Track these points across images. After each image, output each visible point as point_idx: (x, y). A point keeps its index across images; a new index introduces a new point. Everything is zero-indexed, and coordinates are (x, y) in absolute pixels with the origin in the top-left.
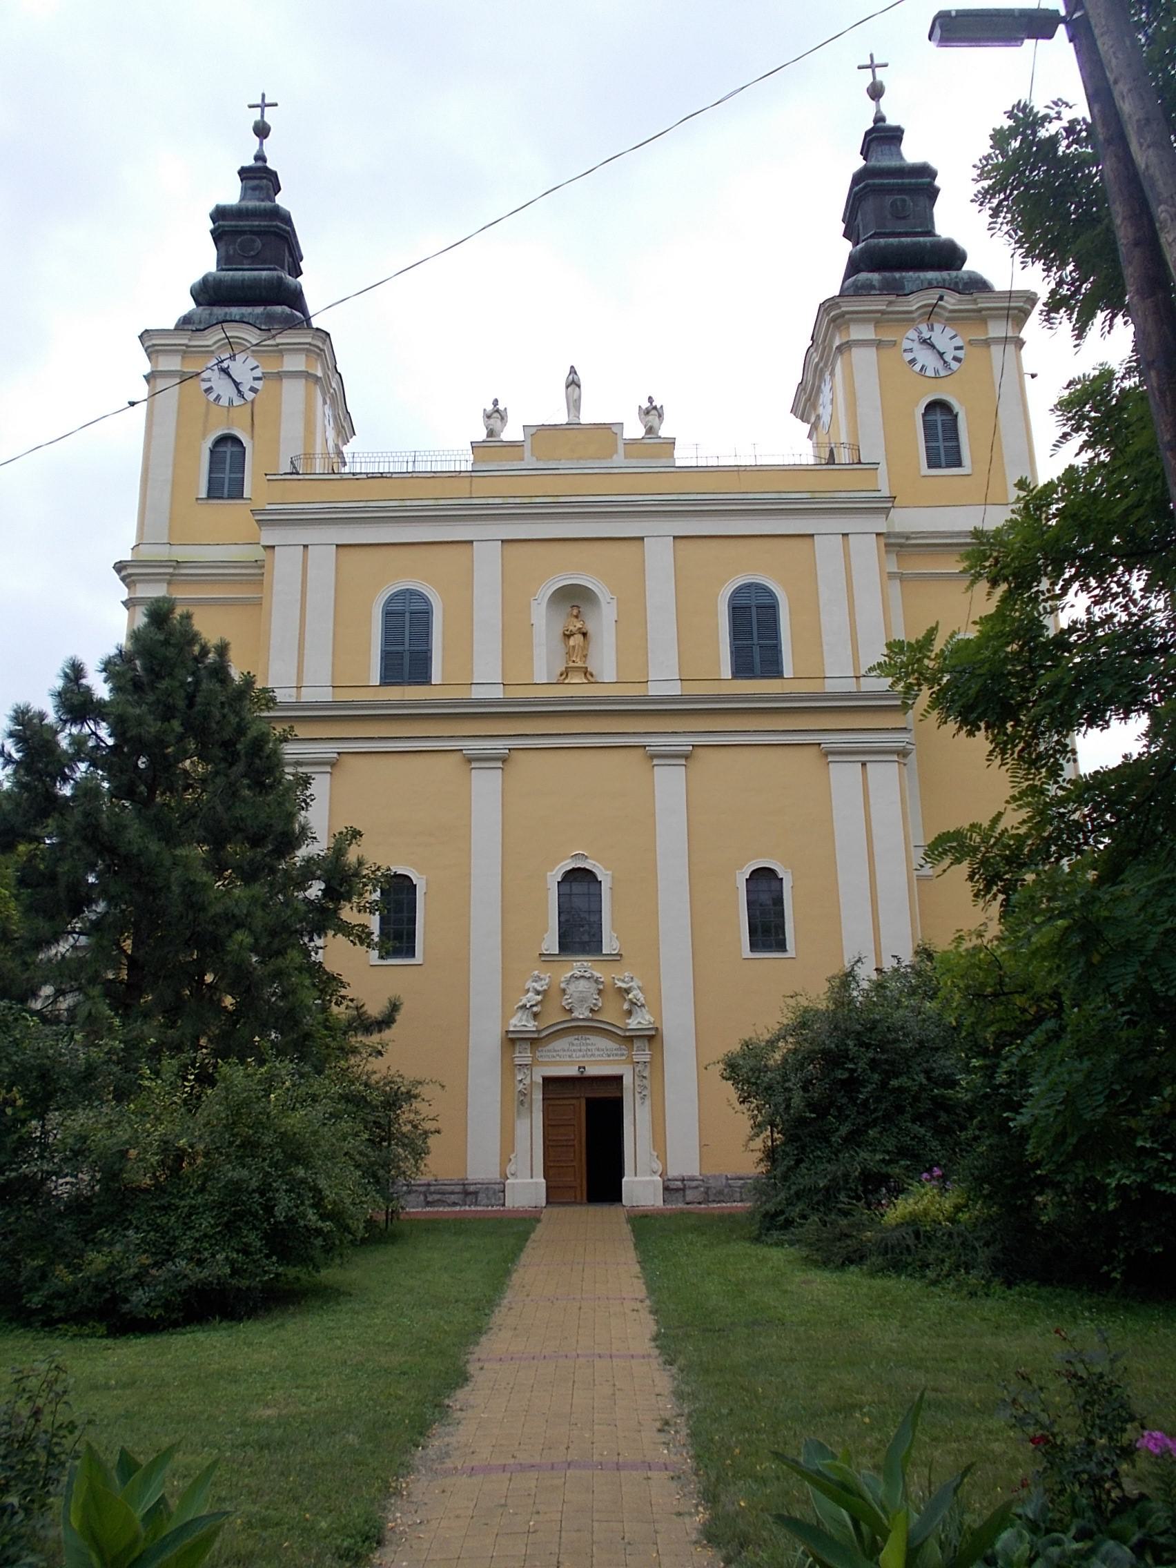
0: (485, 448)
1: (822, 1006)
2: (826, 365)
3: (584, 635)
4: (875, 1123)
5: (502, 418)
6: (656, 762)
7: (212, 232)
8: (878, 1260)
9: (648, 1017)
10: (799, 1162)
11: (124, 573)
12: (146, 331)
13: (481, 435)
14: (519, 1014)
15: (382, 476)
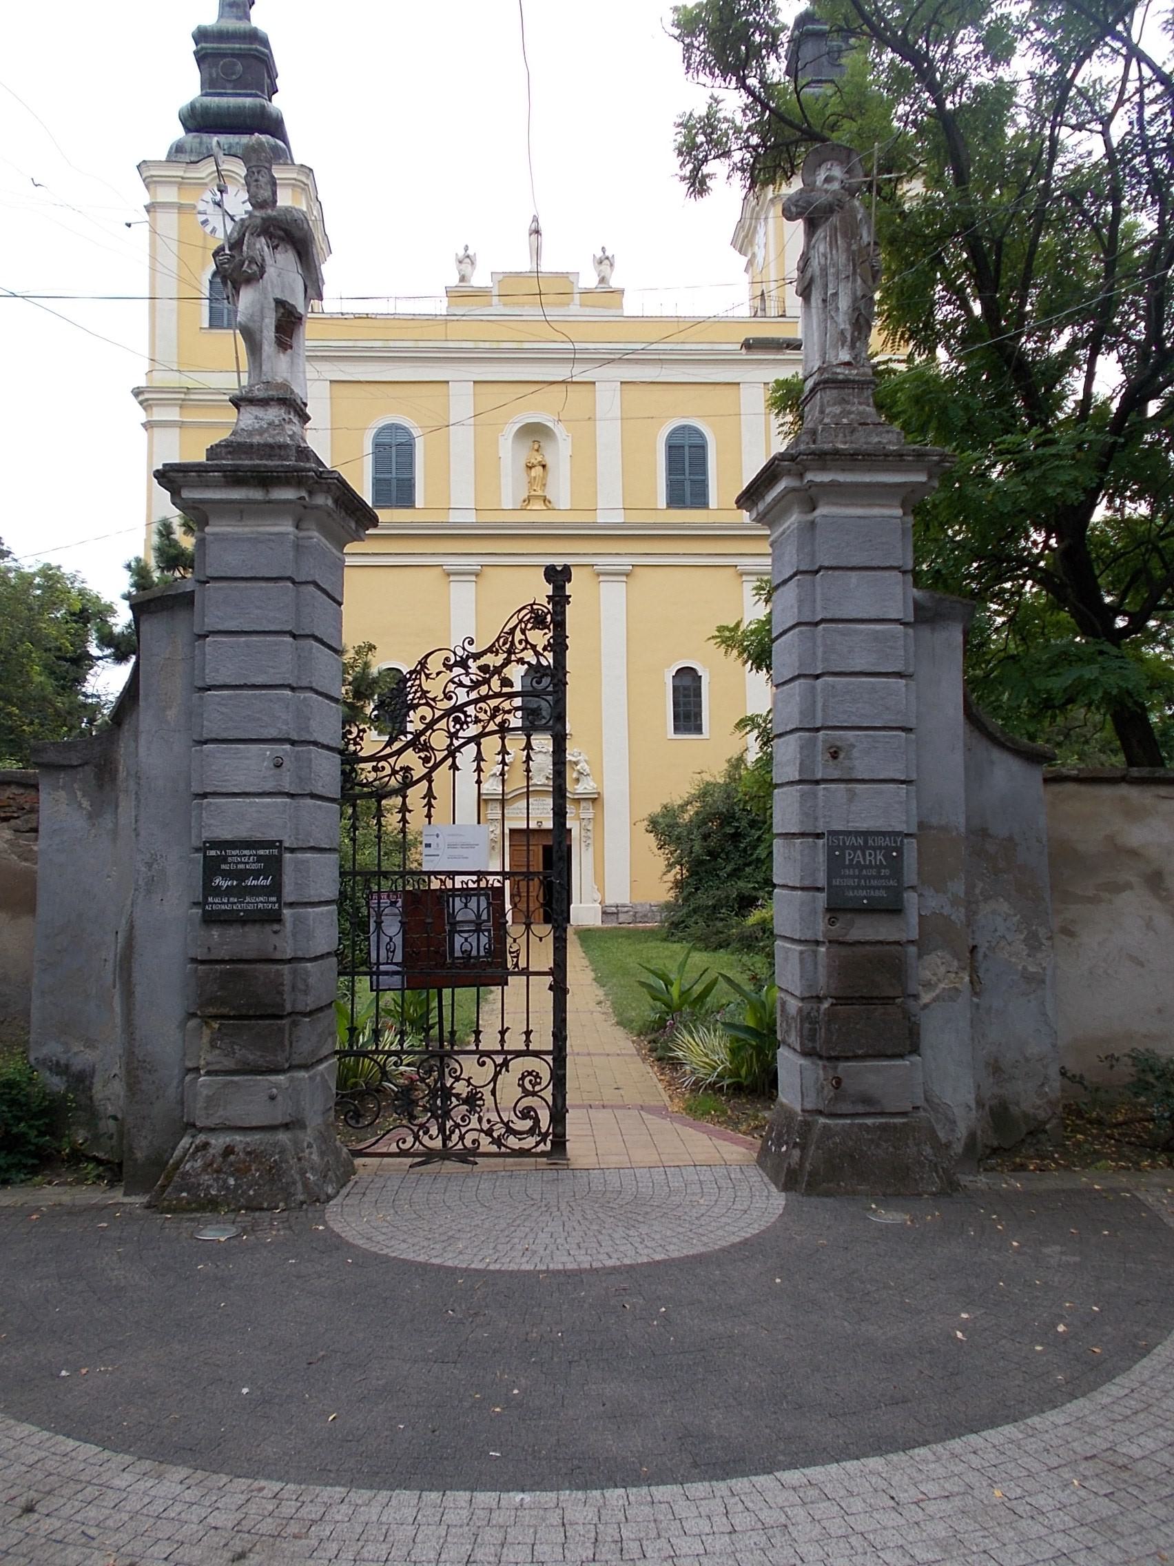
0: (461, 293)
1: (721, 781)
2: (762, 209)
3: (544, 466)
4: (749, 865)
5: (473, 263)
6: (601, 578)
7: (196, 53)
8: (735, 945)
9: (592, 784)
10: (697, 889)
11: (141, 398)
12: (144, 161)
13: (454, 280)
14: (491, 780)
15: (367, 316)
